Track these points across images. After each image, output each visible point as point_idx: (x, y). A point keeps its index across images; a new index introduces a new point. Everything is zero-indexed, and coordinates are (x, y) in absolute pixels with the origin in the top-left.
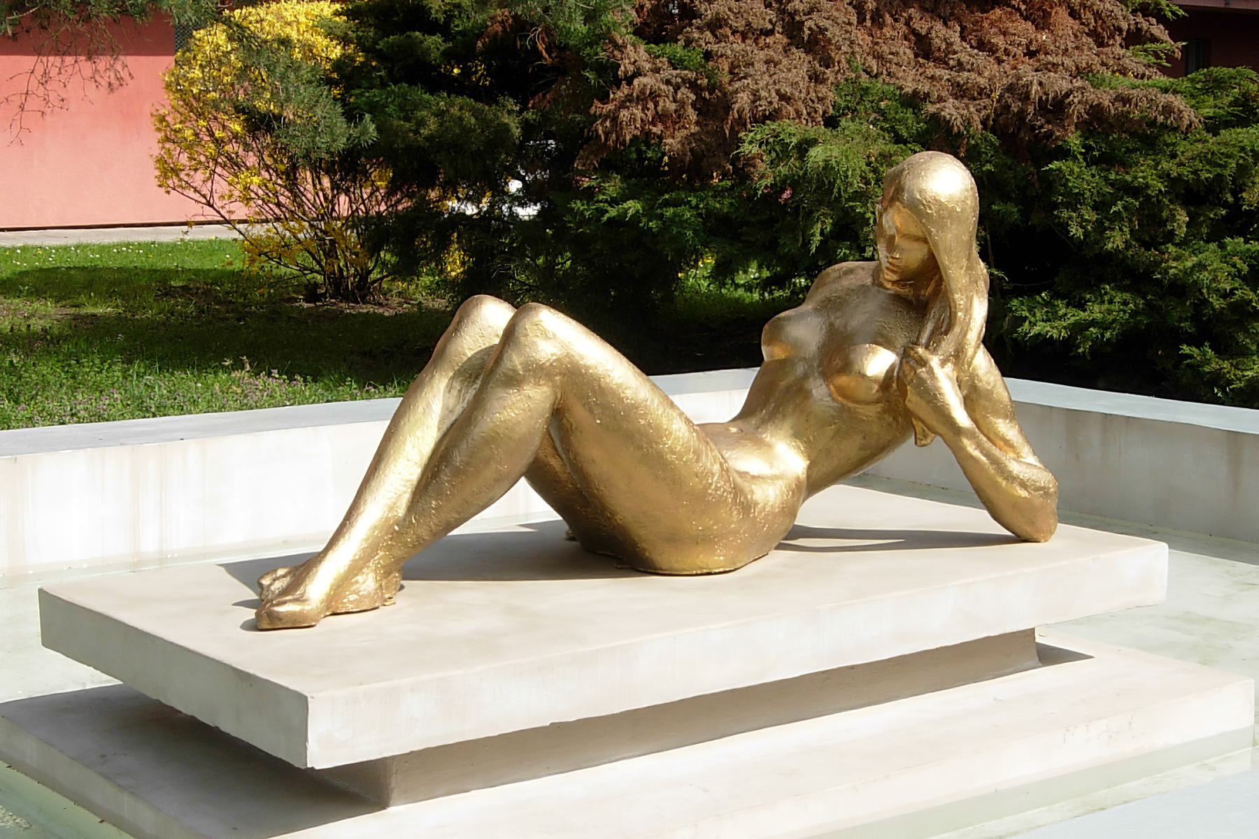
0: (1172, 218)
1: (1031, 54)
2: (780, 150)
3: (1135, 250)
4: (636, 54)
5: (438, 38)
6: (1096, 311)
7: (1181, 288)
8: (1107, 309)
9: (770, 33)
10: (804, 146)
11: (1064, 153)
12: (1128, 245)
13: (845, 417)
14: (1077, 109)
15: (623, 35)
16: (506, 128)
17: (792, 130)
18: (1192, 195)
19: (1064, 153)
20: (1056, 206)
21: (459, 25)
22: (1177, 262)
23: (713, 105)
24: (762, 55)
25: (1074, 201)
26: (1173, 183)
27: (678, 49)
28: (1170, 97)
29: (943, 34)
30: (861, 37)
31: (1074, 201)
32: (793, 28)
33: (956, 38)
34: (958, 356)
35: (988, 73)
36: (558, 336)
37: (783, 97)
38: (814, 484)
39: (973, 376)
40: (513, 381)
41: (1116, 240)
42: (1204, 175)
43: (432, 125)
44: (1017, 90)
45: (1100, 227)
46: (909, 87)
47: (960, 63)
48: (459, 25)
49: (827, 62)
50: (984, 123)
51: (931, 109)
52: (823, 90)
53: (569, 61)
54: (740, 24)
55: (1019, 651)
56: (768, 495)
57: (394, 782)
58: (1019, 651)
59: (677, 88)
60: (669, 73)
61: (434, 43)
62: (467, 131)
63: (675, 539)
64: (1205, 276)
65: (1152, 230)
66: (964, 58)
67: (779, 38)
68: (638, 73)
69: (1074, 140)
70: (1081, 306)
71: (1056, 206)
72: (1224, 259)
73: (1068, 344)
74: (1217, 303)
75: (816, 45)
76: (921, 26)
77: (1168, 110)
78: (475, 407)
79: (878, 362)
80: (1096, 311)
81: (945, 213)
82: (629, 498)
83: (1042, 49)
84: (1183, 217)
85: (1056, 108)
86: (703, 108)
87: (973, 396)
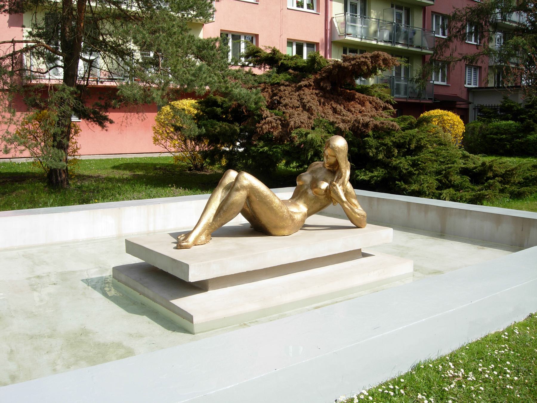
0: (394, 151)
1: (360, 112)
2: (301, 135)
3: (385, 159)
4: (267, 112)
6: (376, 173)
7: (396, 168)
8: (378, 173)
9: (298, 107)
11: (368, 136)
13: (316, 198)
15: (264, 108)
16: (236, 130)
17: (304, 130)
18: (399, 146)
19: (368, 136)
20: (366, 148)
21: (225, 106)
22: (395, 162)
23: (285, 125)
24: (297, 113)
25: (371, 147)
27: (277, 111)
28: (393, 123)
29: (339, 107)
30: (320, 108)
31: (371, 147)
32: (304, 106)
33: (342, 108)
34: (343, 184)
35: (350, 117)
36: (249, 179)
37: (302, 123)
38: (309, 214)
39: (347, 189)
40: (238, 190)
41: (380, 156)
42: (401, 141)
43: (218, 129)
45: (377, 154)
47: (343, 114)
48: (225, 106)
49: (312, 114)
50: (349, 129)
51: (337, 125)
52: (311, 121)
53: (251, 114)
54: (291, 105)
55: (358, 254)
57: (209, 285)
58: (358, 254)
59: (276, 120)
60: (274, 117)
61: (219, 110)
63: (276, 227)
64: (401, 165)
65: (389, 154)
66: (345, 113)
67: (301, 108)
68: (267, 117)
69: (371, 133)
70: (372, 172)
71: (366, 148)
72: (406, 161)
73: (369, 181)
74: (404, 171)
75: (309, 110)
76: (334, 106)
79: (324, 185)
80: (376, 173)
81: (340, 150)
82: (265, 218)
83: (363, 111)
84: (396, 151)
85: (366, 125)
86: (283, 125)
87: (346, 194)
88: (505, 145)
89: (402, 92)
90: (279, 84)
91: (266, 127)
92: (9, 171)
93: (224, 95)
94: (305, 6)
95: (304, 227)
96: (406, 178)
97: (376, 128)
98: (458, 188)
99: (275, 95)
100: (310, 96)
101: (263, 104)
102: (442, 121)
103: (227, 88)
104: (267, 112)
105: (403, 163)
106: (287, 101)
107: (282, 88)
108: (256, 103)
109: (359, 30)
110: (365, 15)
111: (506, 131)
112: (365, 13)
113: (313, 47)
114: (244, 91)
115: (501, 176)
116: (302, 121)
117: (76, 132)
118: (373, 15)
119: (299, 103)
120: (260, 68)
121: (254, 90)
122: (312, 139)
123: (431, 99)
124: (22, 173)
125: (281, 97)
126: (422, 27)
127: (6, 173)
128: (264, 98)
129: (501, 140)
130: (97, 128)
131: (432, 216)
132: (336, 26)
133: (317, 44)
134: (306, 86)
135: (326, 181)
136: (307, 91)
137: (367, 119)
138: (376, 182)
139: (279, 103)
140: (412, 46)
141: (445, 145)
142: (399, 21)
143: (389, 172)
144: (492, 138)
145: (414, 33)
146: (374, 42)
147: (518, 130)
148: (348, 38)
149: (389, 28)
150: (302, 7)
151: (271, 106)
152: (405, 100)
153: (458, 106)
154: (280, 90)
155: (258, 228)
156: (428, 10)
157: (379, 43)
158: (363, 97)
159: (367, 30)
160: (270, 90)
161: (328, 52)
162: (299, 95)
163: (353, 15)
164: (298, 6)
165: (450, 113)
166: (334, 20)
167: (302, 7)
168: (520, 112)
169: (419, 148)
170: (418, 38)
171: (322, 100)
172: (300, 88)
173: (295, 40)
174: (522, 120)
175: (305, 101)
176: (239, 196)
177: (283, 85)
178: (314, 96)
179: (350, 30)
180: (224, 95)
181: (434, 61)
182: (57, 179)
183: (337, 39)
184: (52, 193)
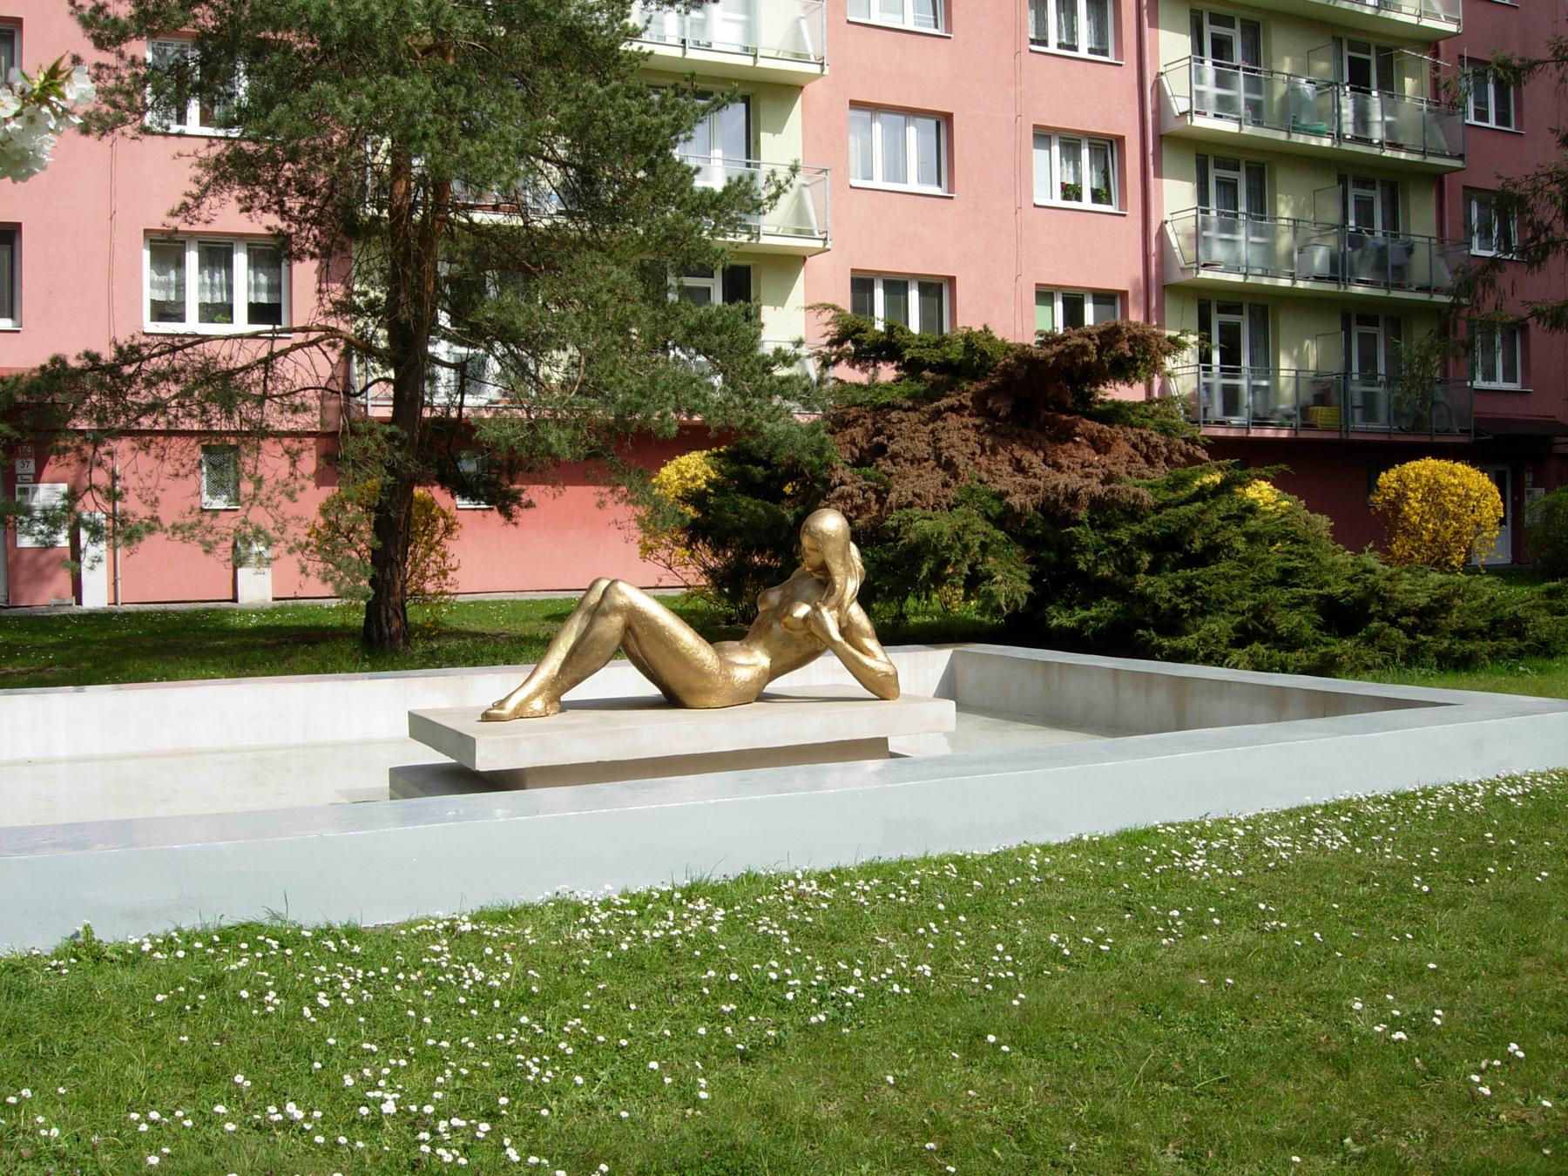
5: (760, 468)
6: (1094, 612)
7: (1142, 598)
8: (1103, 610)
11: (1079, 523)
12: (1114, 574)
16: (783, 516)
18: (1145, 542)
19: (1079, 523)
22: (1142, 582)
25: (1083, 549)
27: (869, 471)
29: (1029, 457)
31: (1083, 549)
32: (938, 457)
34: (839, 605)
37: (915, 495)
39: (849, 618)
40: (605, 614)
41: (1105, 571)
45: (1096, 564)
46: (996, 488)
49: (956, 476)
50: (1036, 508)
54: (909, 456)
55: (875, 748)
58: (875, 748)
59: (865, 492)
61: (758, 471)
62: (761, 517)
66: (1038, 471)
67: (932, 463)
68: (842, 483)
69: (1083, 514)
74: (1164, 606)
75: (949, 466)
76: (1018, 454)
77: (1136, 496)
78: (590, 626)
79: (802, 610)
80: (1094, 612)
85: (1073, 497)
89: (1383, 417)
90: (891, 407)
92: (304, 623)
94: (1087, 194)
95: (763, 697)
96: (1172, 624)
97: (1096, 504)
98: (1290, 642)
99: (879, 432)
100: (959, 435)
102: (1434, 491)
105: (1160, 587)
107: (894, 416)
109: (1244, 251)
110: (1263, 211)
112: (1260, 206)
113: (1113, 304)
115: (1415, 614)
116: (917, 491)
117: (448, 530)
118: (1284, 210)
119: (930, 450)
120: (863, 370)
123: (1468, 432)
124: (328, 628)
125: (890, 438)
126: (1433, 233)
127: (291, 628)
130: (495, 516)
131: (1160, 698)
132: (1175, 244)
133: (1124, 294)
134: (951, 409)
135: (808, 602)
136: (953, 420)
138: (1096, 632)
140: (1399, 287)
141: (1306, 542)
142: (1365, 218)
145: (1410, 250)
146: (1284, 282)
148: (1205, 274)
149: (1332, 242)
150: (1079, 198)
152: (1385, 438)
154: (889, 421)
156: (1452, 187)
157: (1301, 284)
158: (1100, 432)
159: (1269, 250)
160: (869, 422)
161: (1153, 315)
162: (932, 432)
163: (1227, 215)
164: (1066, 197)
165: (1460, 467)
166: (1168, 227)
167: (1079, 198)
170: (1420, 266)
171: (988, 442)
172: (937, 415)
173: (1059, 287)
175: (943, 444)
177: (900, 408)
178: (971, 434)
179: (1219, 252)
181: (1455, 325)
182: (381, 632)
183: (1177, 278)
184: (365, 660)
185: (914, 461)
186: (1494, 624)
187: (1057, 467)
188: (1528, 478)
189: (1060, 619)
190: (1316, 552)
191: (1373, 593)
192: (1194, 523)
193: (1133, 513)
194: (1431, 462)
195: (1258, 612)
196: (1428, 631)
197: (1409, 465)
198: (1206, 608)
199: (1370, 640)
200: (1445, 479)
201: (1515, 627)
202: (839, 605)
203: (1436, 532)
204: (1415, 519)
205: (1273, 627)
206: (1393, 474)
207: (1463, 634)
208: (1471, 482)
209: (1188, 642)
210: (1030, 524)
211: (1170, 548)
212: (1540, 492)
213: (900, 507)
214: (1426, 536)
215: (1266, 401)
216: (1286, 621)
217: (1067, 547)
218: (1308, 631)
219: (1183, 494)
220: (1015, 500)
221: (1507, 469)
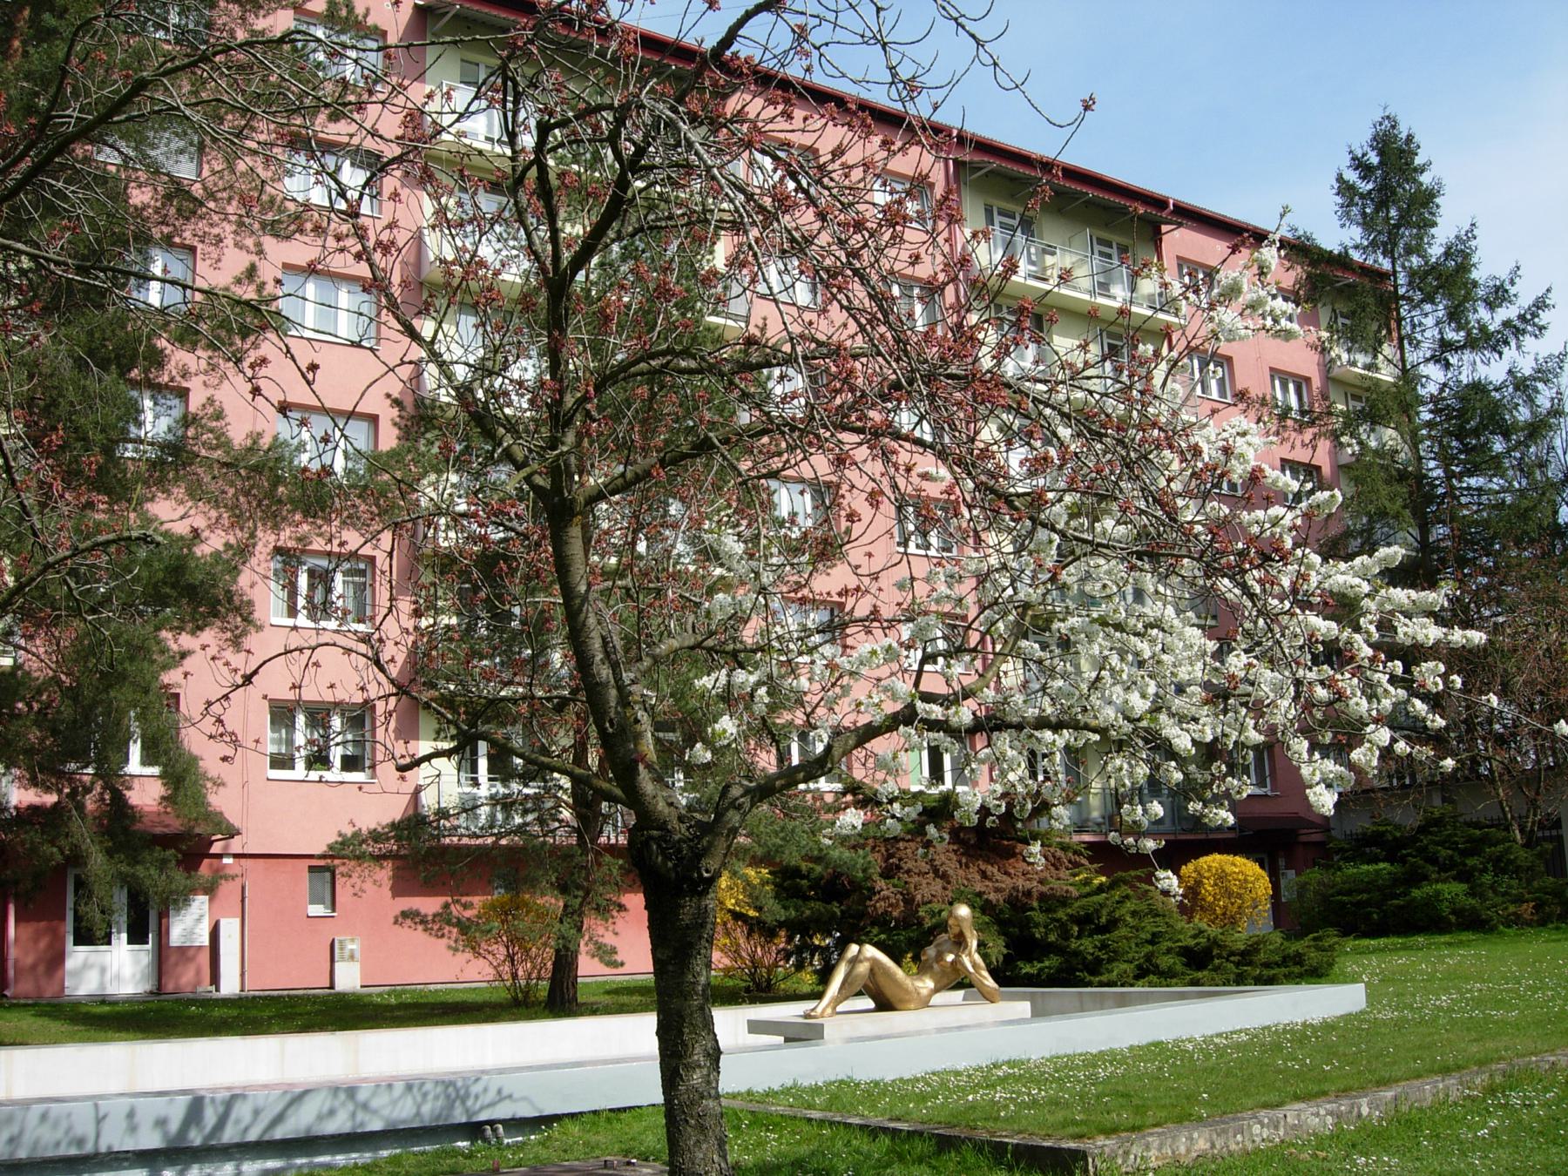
2: (933, 914)
3: (1060, 941)
4: (881, 884)
6: (1047, 963)
7: (1076, 953)
8: (1051, 962)
10: (940, 912)
11: (1033, 909)
13: (943, 972)
14: (1035, 894)
15: (876, 877)
17: (936, 907)
18: (1075, 919)
19: (1033, 909)
21: (812, 876)
23: (909, 900)
25: (1037, 925)
26: (1071, 916)
27: (895, 881)
29: (991, 870)
30: (961, 872)
31: (1037, 925)
32: (936, 871)
34: (970, 955)
35: (1006, 883)
36: (870, 951)
38: (936, 990)
41: (1052, 938)
43: (808, 912)
44: (1015, 888)
48: (812, 876)
53: (856, 886)
56: (924, 992)
63: (901, 1001)
65: (1066, 935)
69: (1035, 904)
75: (944, 877)
76: (983, 867)
79: (950, 958)
80: (1047, 963)
81: (963, 919)
82: (889, 991)
85: (1028, 894)
86: (906, 901)
87: (974, 965)
88: (1371, 913)
91: (881, 905)
93: (818, 860)
97: (1043, 897)
99: (891, 856)
101: (875, 871)
102: (1222, 877)
103: (821, 850)
104: (881, 884)
105: (1087, 945)
106: (910, 865)
107: (901, 845)
108: (864, 871)
111: (1370, 885)
114: (847, 854)
121: (861, 852)
122: (162, 351)
125: (900, 860)
128: (876, 861)
129: (1359, 904)
137: (1028, 885)
139: (899, 868)
143: (1067, 961)
144: (1340, 902)
147: (1395, 881)
151: (888, 873)
153: (1303, 839)
155: (884, 1004)
165: (1239, 860)
168: (1400, 843)
169: (1113, 924)
174: (1403, 860)
176: (863, 968)
178: (952, 855)
180: (818, 860)
185: (921, 874)
186: (1285, 959)
187: (1007, 873)
188: (1282, 862)
189: (1027, 969)
190: (1171, 922)
191: (1215, 943)
192: (1102, 906)
193: (1064, 901)
194: (1217, 857)
195: (1149, 957)
196: (1250, 964)
197: (1202, 860)
198: (1116, 956)
199: (1216, 969)
200: (1229, 869)
201: (1298, 959)
202: (970, 955)
203: (1225, 907)
204: (1210, 899)
205: (1157, 966)
206: (1191, 866)
207: (1267, 965)
208: (1245, 868)
209: (1104, 978)
210: (1001, 911)
211: (1087, 922)
212: (1291, 874)
213: (925, 903)
214: (1219, 911)
215: (1080, 813)
216: (1165, 962)
217: (1027, 924)
218: (1179, 968)
219: (1088, 889)
220: (992, 897)
221: (1264, 856)
